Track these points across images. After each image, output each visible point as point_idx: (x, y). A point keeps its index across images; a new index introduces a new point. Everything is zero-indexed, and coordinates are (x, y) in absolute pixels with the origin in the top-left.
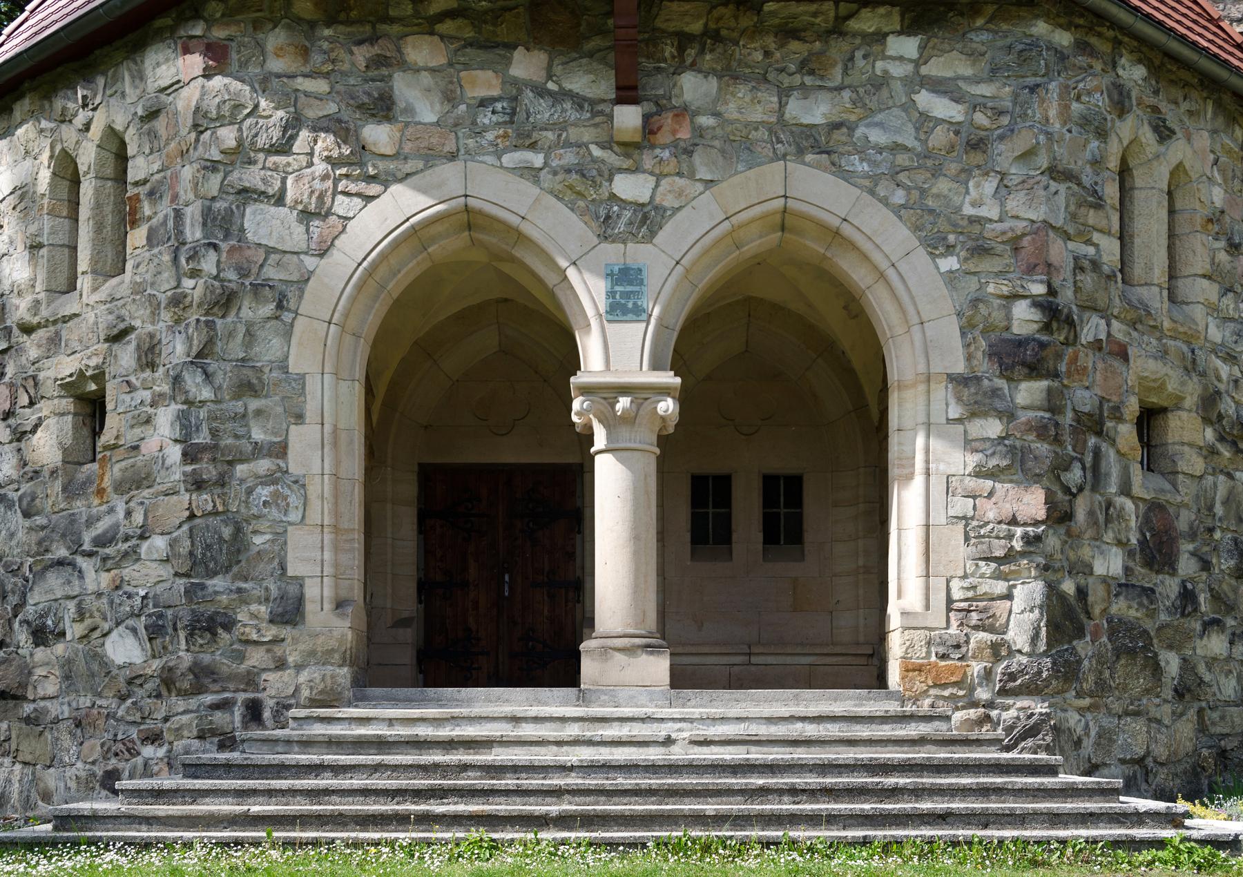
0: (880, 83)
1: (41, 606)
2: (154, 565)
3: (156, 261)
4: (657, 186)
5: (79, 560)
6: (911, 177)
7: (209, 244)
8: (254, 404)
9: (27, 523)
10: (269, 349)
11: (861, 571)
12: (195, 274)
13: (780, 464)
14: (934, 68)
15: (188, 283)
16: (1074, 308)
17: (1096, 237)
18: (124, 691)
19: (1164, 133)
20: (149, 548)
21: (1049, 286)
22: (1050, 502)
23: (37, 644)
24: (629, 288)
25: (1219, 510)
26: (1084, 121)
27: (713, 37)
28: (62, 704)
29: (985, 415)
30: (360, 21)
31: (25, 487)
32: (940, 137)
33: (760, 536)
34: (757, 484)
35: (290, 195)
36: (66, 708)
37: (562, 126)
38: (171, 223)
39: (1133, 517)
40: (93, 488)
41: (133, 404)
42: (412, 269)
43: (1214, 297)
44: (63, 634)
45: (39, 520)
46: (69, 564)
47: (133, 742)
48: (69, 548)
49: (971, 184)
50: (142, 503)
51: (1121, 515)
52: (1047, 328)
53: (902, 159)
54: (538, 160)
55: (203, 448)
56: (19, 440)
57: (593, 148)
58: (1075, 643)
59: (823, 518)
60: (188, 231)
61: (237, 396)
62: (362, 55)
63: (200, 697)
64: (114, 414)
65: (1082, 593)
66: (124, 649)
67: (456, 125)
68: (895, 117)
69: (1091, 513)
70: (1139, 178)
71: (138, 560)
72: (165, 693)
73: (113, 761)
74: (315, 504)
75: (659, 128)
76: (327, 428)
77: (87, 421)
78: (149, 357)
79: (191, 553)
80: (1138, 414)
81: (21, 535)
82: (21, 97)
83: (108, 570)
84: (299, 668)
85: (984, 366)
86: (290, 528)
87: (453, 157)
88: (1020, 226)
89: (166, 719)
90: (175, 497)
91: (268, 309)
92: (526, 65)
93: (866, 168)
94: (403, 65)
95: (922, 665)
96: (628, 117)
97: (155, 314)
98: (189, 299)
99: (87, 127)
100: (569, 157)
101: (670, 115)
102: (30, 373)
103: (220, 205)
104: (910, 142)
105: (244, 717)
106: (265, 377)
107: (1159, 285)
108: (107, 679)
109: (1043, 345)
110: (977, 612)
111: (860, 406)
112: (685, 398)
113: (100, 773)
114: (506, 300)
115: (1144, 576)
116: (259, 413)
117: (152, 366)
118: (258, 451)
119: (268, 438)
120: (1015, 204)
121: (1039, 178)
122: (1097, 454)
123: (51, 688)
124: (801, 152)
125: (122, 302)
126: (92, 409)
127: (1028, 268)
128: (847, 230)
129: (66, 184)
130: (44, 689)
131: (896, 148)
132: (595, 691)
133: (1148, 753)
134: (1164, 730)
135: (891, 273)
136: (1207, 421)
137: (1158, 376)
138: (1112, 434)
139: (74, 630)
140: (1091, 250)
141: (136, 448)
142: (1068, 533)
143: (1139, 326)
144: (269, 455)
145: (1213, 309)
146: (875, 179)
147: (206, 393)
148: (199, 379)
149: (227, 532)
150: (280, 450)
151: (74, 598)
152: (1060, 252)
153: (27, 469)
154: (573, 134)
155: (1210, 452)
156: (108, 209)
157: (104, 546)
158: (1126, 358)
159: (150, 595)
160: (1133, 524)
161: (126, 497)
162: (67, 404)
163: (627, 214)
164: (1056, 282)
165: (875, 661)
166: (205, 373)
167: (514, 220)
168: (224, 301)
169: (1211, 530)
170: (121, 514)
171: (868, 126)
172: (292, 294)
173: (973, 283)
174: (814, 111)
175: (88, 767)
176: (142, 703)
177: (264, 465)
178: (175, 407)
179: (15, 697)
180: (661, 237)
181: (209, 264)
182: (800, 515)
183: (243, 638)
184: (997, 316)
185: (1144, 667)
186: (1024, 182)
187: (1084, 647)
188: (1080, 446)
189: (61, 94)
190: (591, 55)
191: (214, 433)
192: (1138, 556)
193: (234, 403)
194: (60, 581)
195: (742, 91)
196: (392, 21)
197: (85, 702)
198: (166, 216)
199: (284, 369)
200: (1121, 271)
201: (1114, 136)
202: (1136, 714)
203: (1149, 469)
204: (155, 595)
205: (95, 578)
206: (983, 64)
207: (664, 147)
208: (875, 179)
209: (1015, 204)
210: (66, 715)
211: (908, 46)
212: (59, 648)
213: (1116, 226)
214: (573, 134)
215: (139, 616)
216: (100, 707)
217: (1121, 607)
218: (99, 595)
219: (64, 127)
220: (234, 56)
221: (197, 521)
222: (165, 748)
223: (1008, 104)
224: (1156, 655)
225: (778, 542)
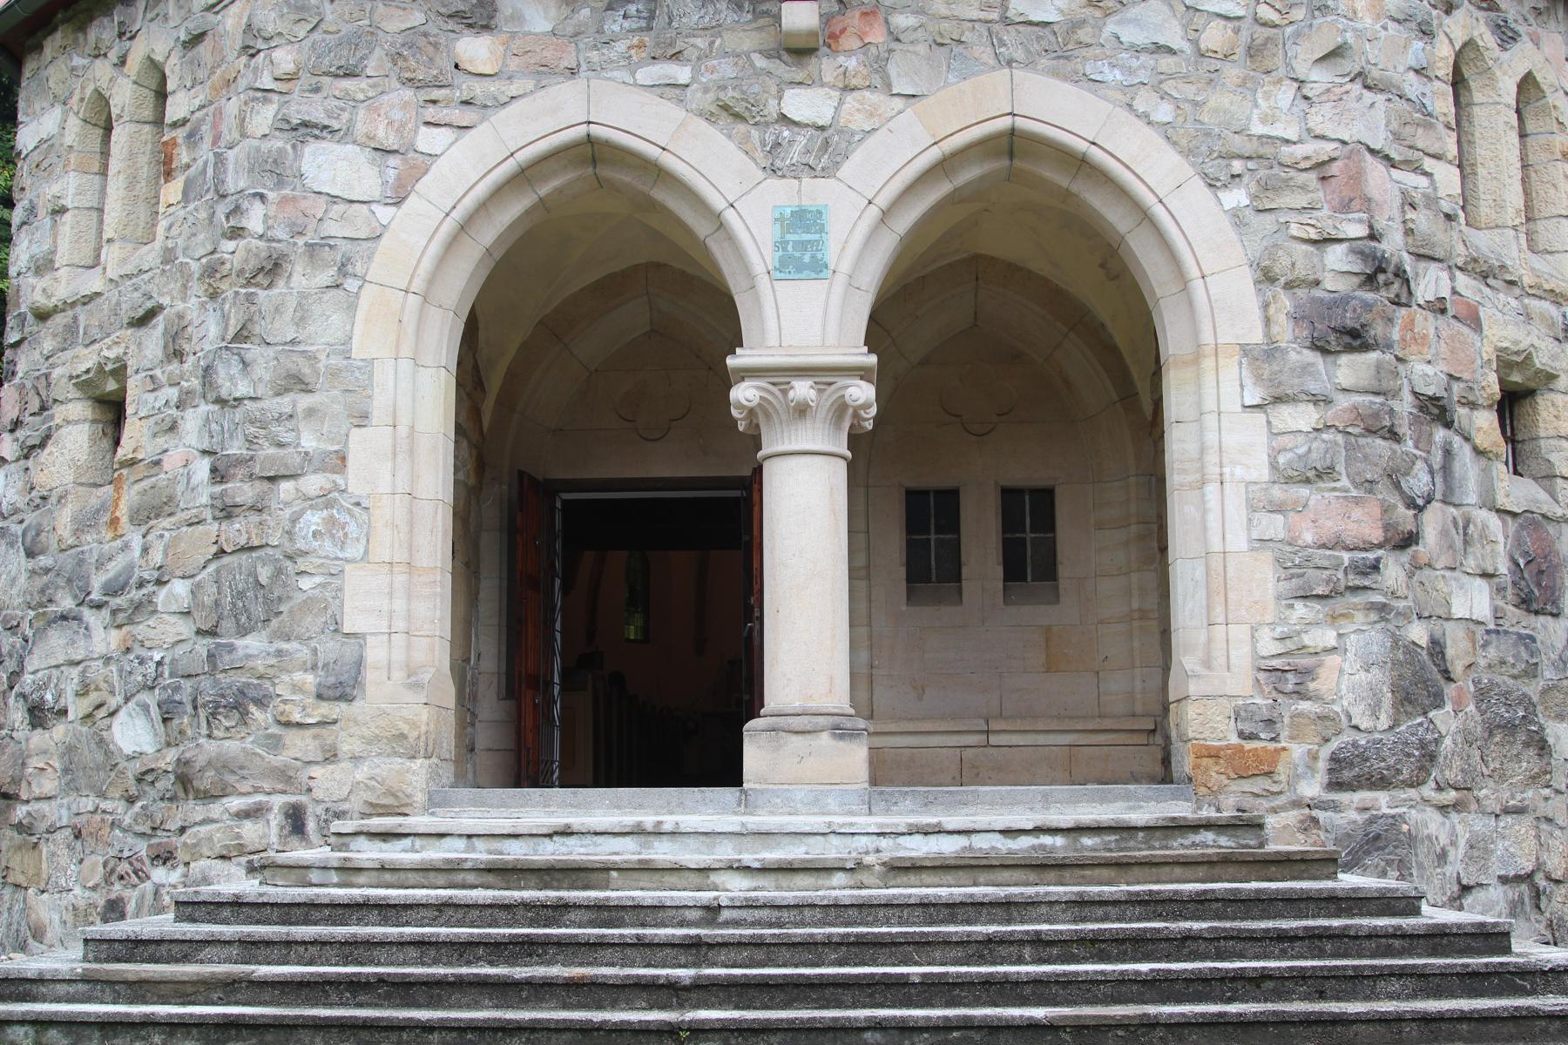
1: (40, 674)
2: (173, 619)
3: (191, 219)
4: (841, 102)
5: (86, 613)
7: (255, 195)
8: (304, 401)
9: (31, 564)
10: (326, 328)
11: (1136, 615)
12: (236, 233)
13: (1022, 474)
16: (1405, 255)
17: (1428, 164)
18: (133, 791)
20: (167, 596)
21: (1371, 227)
23: (34, 726)
24: (806, 237)
28: (61, 806)
31: (31, 518)
33: (999, 571)
36: (64, 812)
38: (210, 171)
39: (1501, 539)
40: (106, 518)
41: (157, 405)
45: (44, 561)
46: (74, 618)
47: (140, 860)
48: (75, 597)
49: (1259, 95)
50: (162, 536)
52: (1370, 280)
53: (1166, 63)
54: (682, 74)
55: (240, 461)
56: (26, 457)
57: (756, 58)
58: (1431, 715)
59: (1085, 545)
60: (230, 179)
63: (225, 800)
64: (135, 419)
66: (133, 734)
67: (576, 34)
69: (1444, 533)
71: (155, 612)
72: (181, 794)
73: (117, 886)
75: (843, 31)
76: (403, 430)
77: (109, 431)
79: (217, 603)
80: (1498, 397)
81: (22, 579)
82: (54, 30)
83: (119, 627)
85: (1284, 330)
86: (348, 567)
87: (573, 72)
88: (1328, 149)
89: (183, 830)
90: (200, 527)
93: (1119, 77)
95: (1220, 748)
98: (228, 266)
99: (122, 62)
101: (857, 14)
102: (44, 371)
104: (1177, 42)
105: (282, 828)
106: (321, 365)
107: (1514, 228)
108: (113, 774)
110: (1289, 675)
111: (1128, 396)
112: (883, 378)
113: (102, 902)
114: (658, 266)
116: (311, 412)
119: (322, 446)
121: (1348, 87)
122: (1448, 453)
123: (48, 785)
125: (146, 277)
126: (112, 411)
127: (1341, 203)
129: (99, 132)
130: (40, 786)
131: (1159, 49)
132: (762, 792)
133: (1539, 866)
134: (1558, 833)
137: (1522, 347)
138: (1465, 423)
139: (77, 708)
140: (1423, 182)
141: (157, 463)
143: (1490, 281)
146: (1125, 88)
148: (236, 368)
151: (79, 663)
152: (1378, 178)
153: (34, 493)
156: (143, 160)
157: (115, 594)
159: (167, 660)
160: (1500, 548)
161: (144, 529)
163: (802, 140)
164: (1381, 223)
165: (1158, 739)
166: (244, 363)
167: (652, 151)
171: (1120, 23)
175: (87, 893)
176: (153, 808)
180: (846, 170)
182: (1053, 543)
183: (283, 719)
185: (1527, 745)
186: (1328, 90)
187: (1445, 719)
188: (1424, 441)
189: (96, 23)
192: (1510, 591)
193: (278, 399)
194: (62, 641)
197: (88, 803)
198: (206, 163)
200: (1463, 208)
201: (1442, 37)
202: (1520, 811)
203: (1516, 472)
204: (173, 661)
205: (103, 638)
207: (849, 53)
210: (65, 822)
213: (1452, 150)
214: (730, 40)
215: (152, 688)
216: (104, 812)
218: (107, 660)
219: (98, 62)
221: (226, 560)
222: (181, 870)
224: (1542, 728)
225: (1025, 579)
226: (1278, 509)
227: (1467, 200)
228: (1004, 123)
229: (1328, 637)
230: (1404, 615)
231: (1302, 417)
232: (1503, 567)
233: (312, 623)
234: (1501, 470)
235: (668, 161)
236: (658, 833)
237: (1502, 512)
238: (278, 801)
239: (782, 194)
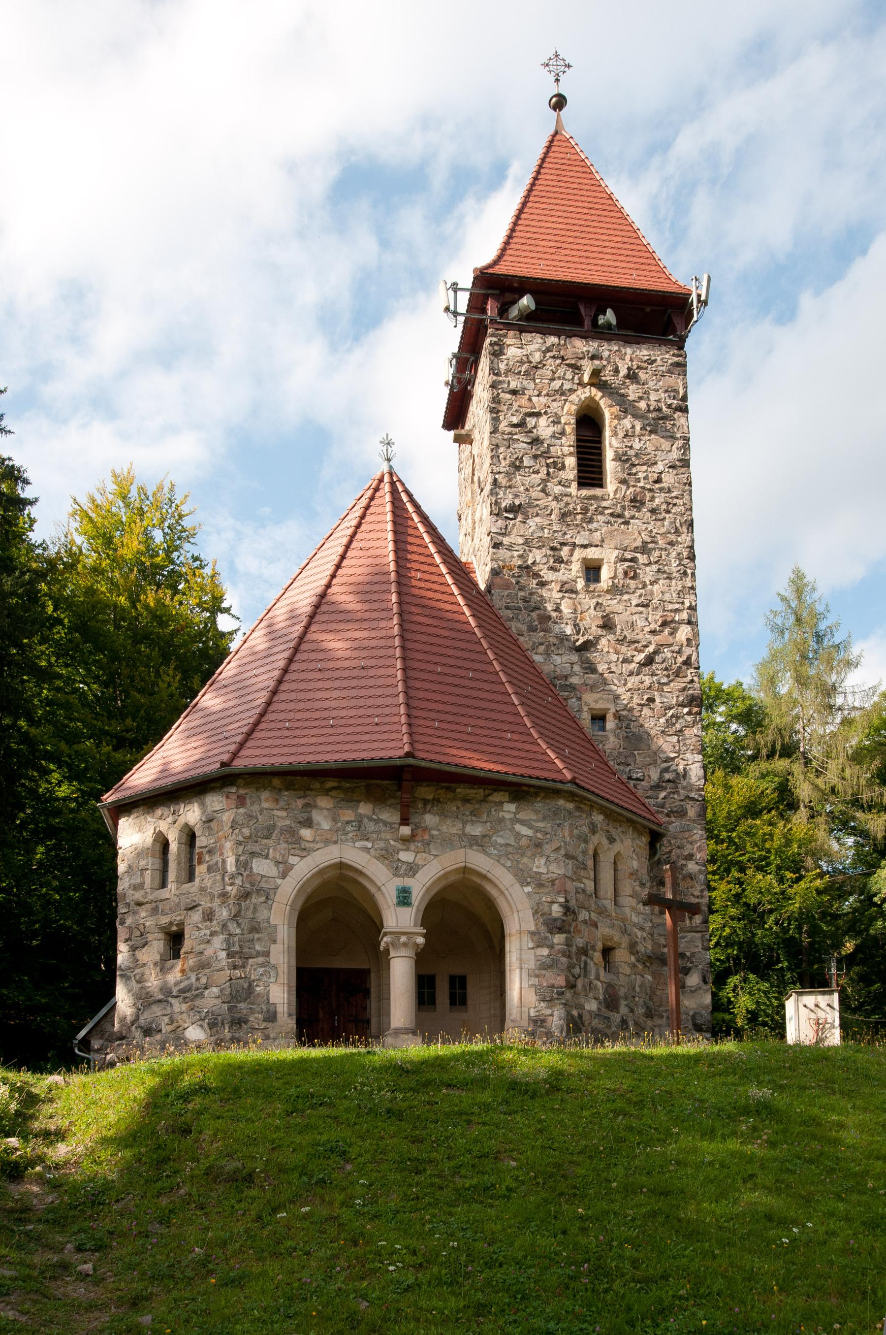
0: (502, 820)
5: (170, 999)
6: (513, 855)
8: (257, 936)
10: (262, 915)
12: (232, 884)
13: (457, 971)
14: (522, 816)
15: (229, 888)
17: (584, 880)
19: (612, 840)
22: (567, 981)
25: (637, 989)
26: (579, 837)
27: (437, 801)
29: (542, 947)
30: (299, 790)
32: (524, 842)
33: (448, 1002)
34: (447, 979)
37: (379, 832)
42: (316, 882)
43: (634, 904)
44: (160, 1031)
51: (596, 987)
52: (565, 914)
53: (510, 849)
54: (369, 845)
55: (237, 952)
61: (250, 933)
62: (300, 803)
65: (580, 1016)
68: (507, 833)
69: (584, 986)
70: (602, 857)
74: (281, 974)
78: (209, 916)
85: (543, 929)
87: (336, 842)
91: (263, 899)
92: (365, 809)
94: (315, 807)
96: (406, 830)
97: (212, 900)
100: (382, 844)
109: (563, 921)
112: (425, 936)
115: (606, 1013)
116: (258, 939)
117: (211, 920)
118: (258, 954)
120: (553, 867)
122: (586, 963)
124: (471, 846)
128: (489, 875)
131: (508, 845)
135: (506, 892)
136: (632, 953)
139: (165, 1029)
142: (575, 993)
144: (263, 956)
145: (634, 909)
146: (500, 856)
147: (238, 931)
149: (246, 985)
150: (267, 954)
152: (570, 886)
154: (383, 836)
158: (597, 927)
162: (161, 936)
163: (405, 867)
164: (569, 898)
168: (246, 895)
169: (634, 997)
170: (193, 979)
172: (271, 893)
174: (476, 830)
177: (261, 960)
178: (222, 937)
181: (238, 881)
184: (546, 909)
190: (390, 806)
191: (241, 947)
195: (449, 821)
196: (312, 790)
199: (269, 922)
206: (541, 816)
208: (500, 856)
209: (553, 867)
211: (512, 807)
213: (592, 876)
214: (383, 836)
217: (595, 1022)
218: (182, 1013)
220: (248, 801)
223: (549, 830)
226: (537, 976)
229: (549, 1012)
230: (571, 1006)
235: (364, 870)
239: (399, 882)
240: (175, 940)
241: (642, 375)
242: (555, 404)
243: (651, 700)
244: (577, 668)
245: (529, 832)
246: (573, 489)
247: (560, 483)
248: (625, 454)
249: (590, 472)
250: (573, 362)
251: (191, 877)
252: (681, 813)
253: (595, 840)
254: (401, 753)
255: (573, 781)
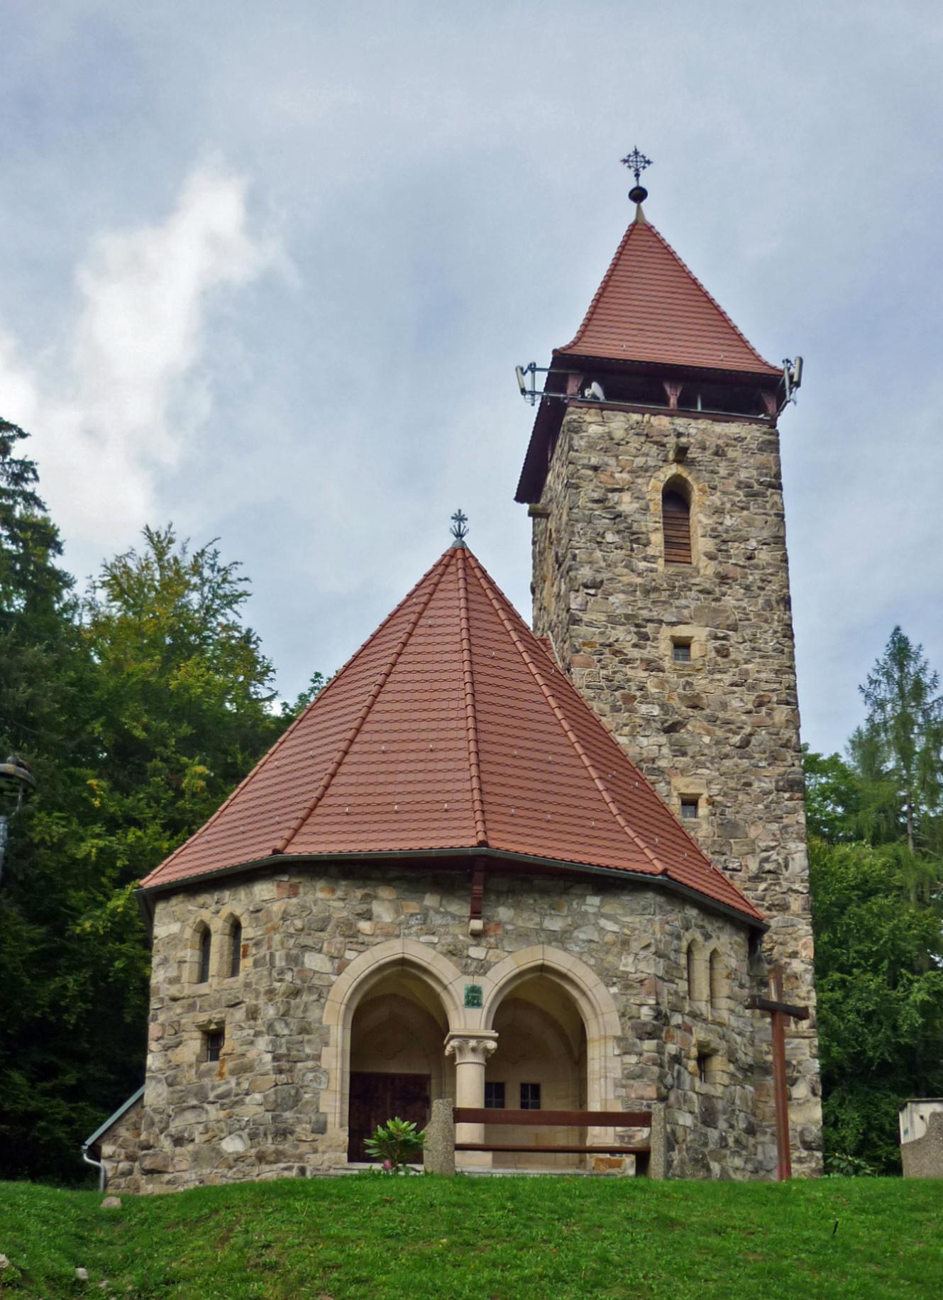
5: (205, 1105)
8: (307, 1037)
10: (313, 1014)
12: (281, 980)
13: (532, 1079)
14: (606, 910)
15: (277, 985)
19: (707, 937)
23: (176, 1146)
25: (738, 1102)
35: (325, 949)
37: (446, 925)
44: (193, 1140)
51: (691, 1101)
52: (656, 1018)
53: (593, 946)
54: (435, 940)
55: (283, 1055)
62: (359, 893)
69: (677, 1098)
78: (253, 1014)
84: (324, 1152)
85: (630, 1033)
87: (398, 936)
88: (644, 976)
92: (430, 900)
94: (376, 897)
96: (477, 924)
103: (294, 952)
116: (309, 1041)
117: (255, 1019)
118: (308, 1058)
120: (642, 966)
122: (679, 1072)
123: (184, 1166)
131: (591, 941)
146: (581, 953)
147: (286, 1032)
149: (293, 1092)
150: (318, 1057)
155: (732, 1076)
162: (198, 1035)
163: (475, 964)
168: (296, 993)
172: (325, 990)
173: (624, 998)
174: (555, 924)
177: (310, 1064)
179: (159, 1172)
180: (489, 974)
188: (671, 1068)
191: (288, 1049)
199: (321, 1023)
212: (190, 1147)
213: (686, 976)
214: (451, 930)
218: (218, 1121)
226: (624, 1086)
227: (690, 992)
228: (540, 962)
231: (633, 1059)
232: (697, 1110)
233: (309, 1108)
234: (697, 1080)
236: (680, 623)
237: (697, 1093)
238: (296, 1165)
239: (468, 981)
240: (213, 1038)
241: (731, 453)
242: (640, 481)
243: (749, 785)
244: (665, 751)
245: (615, 928)
246: (660, 565)
247: (645, 559)
248: (714, 530)
249: (677, 546)
250: (658, 439)
251: (234, 971)
252: (784, 907)
253: (688, 936)
254: (474, 842)
255: (664, 873)
